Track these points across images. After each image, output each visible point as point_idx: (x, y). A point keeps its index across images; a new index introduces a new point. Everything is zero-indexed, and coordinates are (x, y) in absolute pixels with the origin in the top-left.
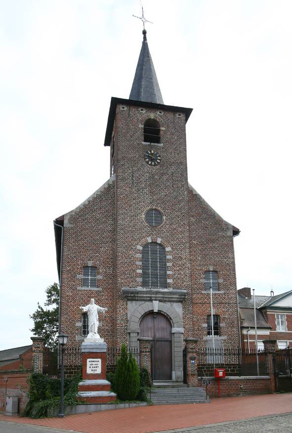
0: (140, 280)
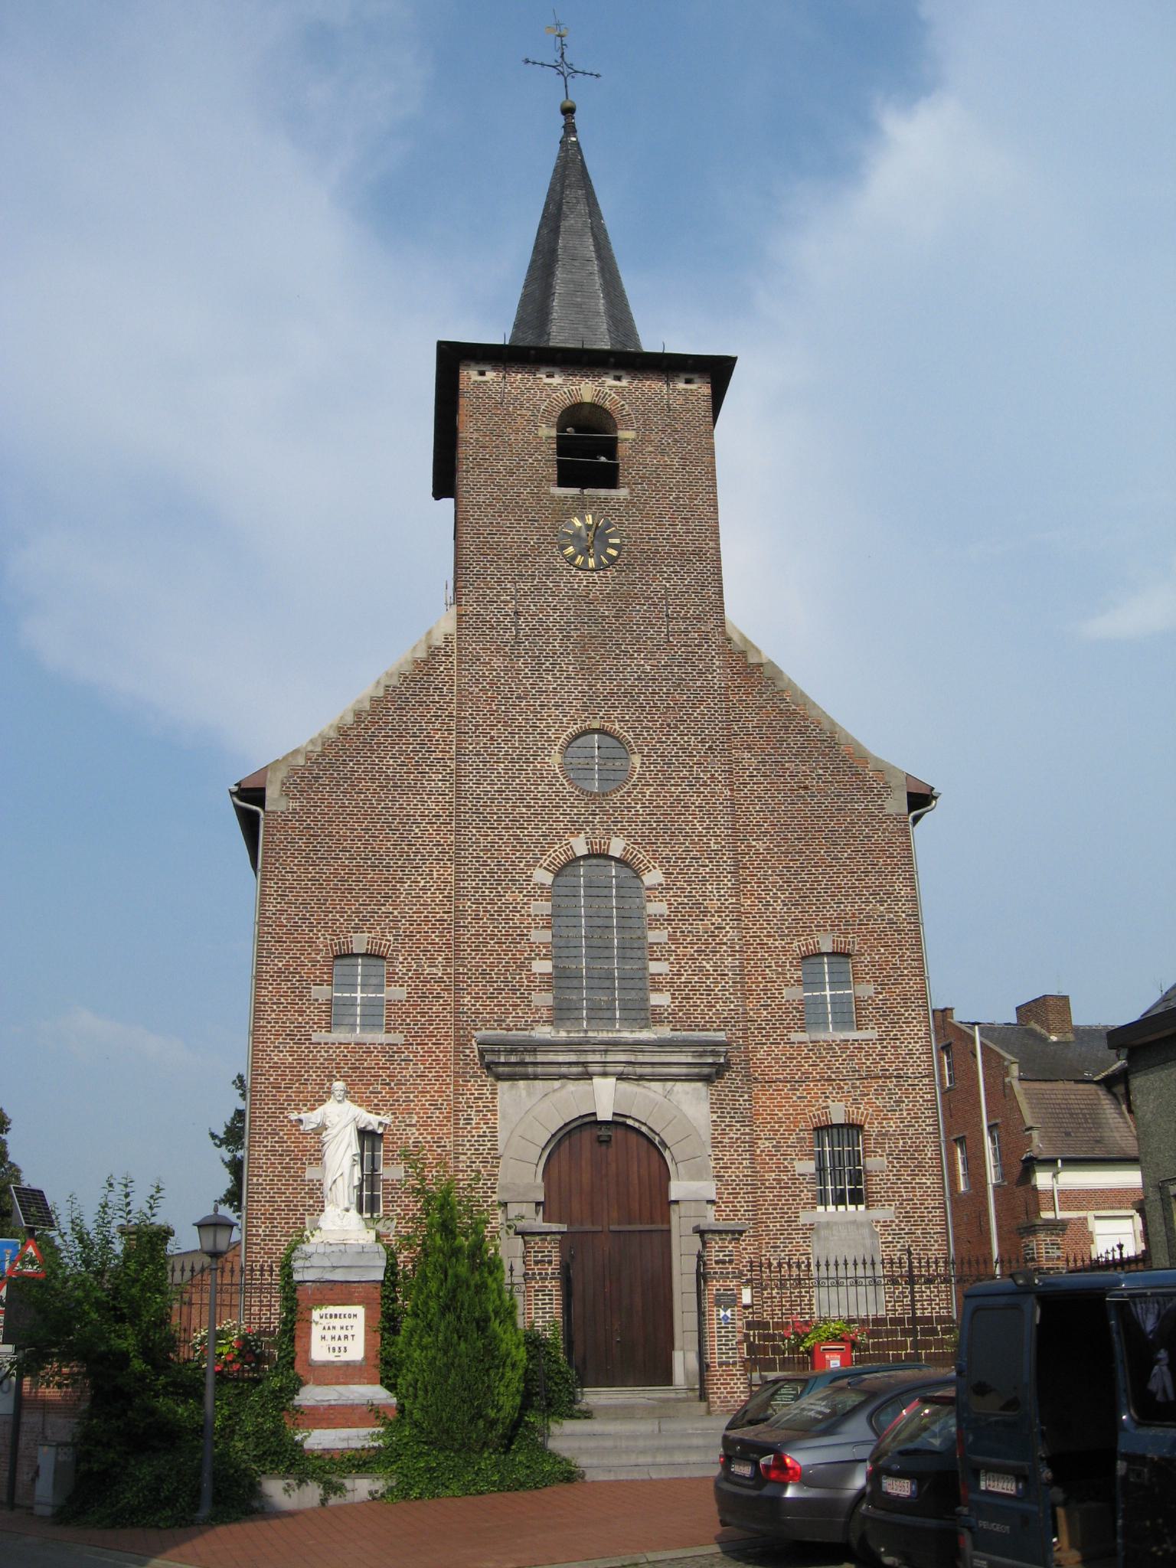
0: (543, 999)
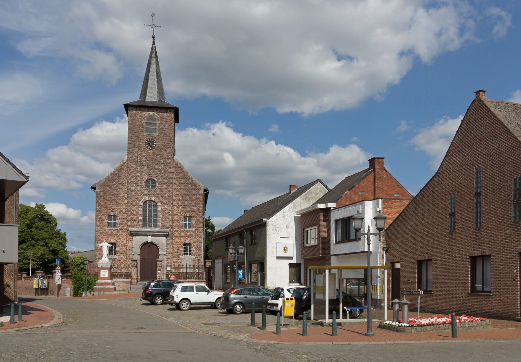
0: (141, 223)
